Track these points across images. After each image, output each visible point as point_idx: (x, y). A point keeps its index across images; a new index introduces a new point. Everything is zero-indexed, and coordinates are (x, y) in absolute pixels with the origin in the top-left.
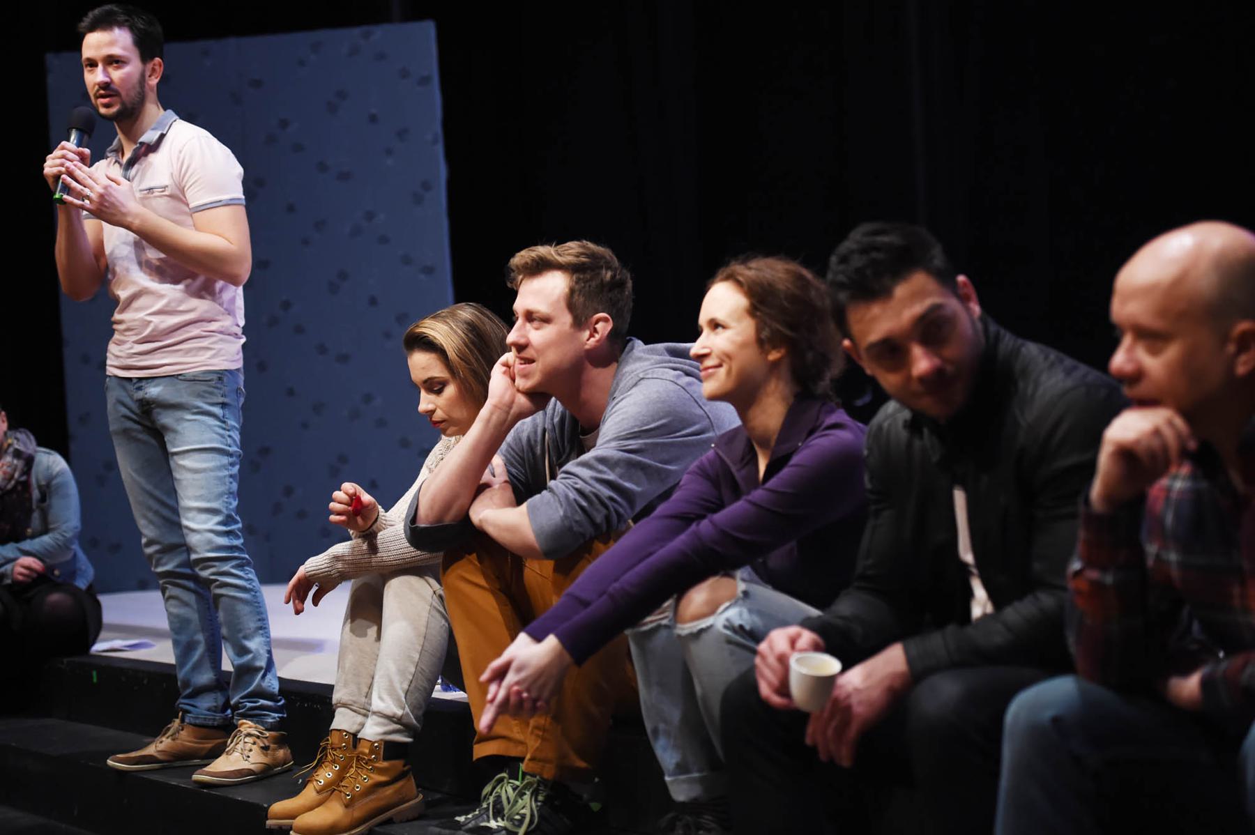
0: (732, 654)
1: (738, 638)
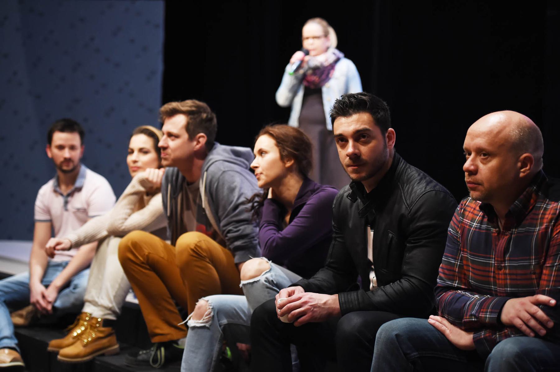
0: (269, 293)
1: (271, 286)
